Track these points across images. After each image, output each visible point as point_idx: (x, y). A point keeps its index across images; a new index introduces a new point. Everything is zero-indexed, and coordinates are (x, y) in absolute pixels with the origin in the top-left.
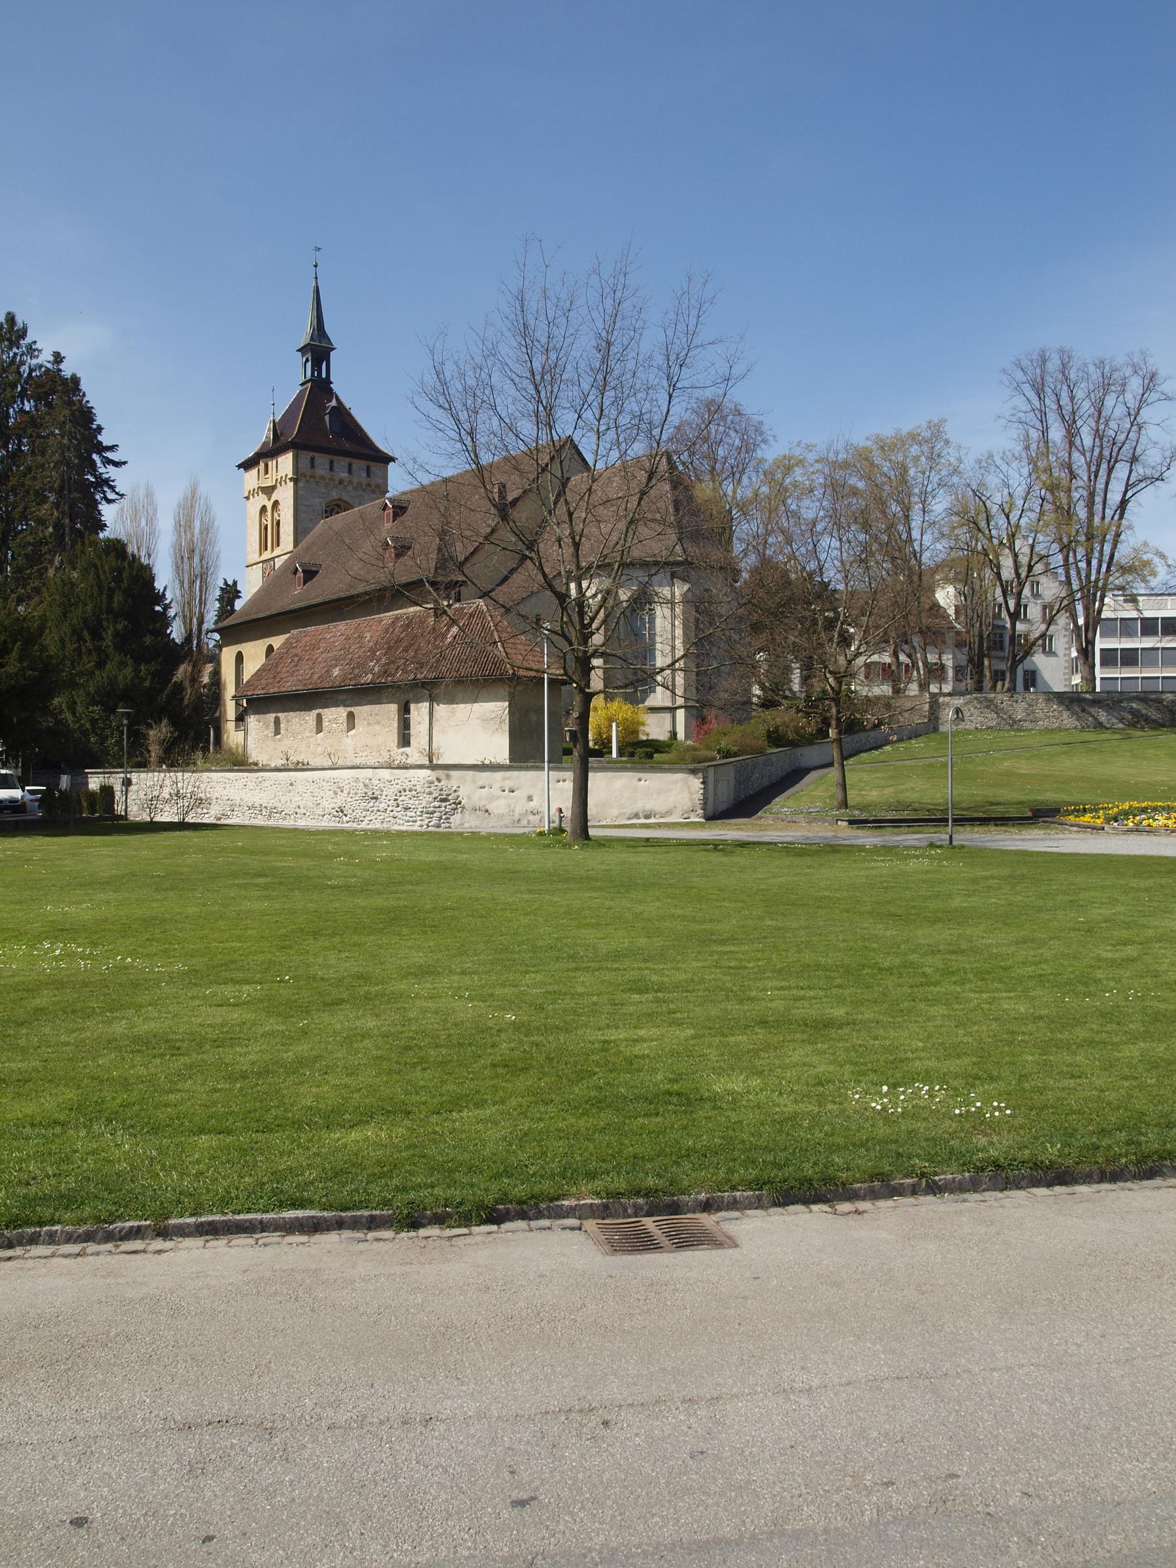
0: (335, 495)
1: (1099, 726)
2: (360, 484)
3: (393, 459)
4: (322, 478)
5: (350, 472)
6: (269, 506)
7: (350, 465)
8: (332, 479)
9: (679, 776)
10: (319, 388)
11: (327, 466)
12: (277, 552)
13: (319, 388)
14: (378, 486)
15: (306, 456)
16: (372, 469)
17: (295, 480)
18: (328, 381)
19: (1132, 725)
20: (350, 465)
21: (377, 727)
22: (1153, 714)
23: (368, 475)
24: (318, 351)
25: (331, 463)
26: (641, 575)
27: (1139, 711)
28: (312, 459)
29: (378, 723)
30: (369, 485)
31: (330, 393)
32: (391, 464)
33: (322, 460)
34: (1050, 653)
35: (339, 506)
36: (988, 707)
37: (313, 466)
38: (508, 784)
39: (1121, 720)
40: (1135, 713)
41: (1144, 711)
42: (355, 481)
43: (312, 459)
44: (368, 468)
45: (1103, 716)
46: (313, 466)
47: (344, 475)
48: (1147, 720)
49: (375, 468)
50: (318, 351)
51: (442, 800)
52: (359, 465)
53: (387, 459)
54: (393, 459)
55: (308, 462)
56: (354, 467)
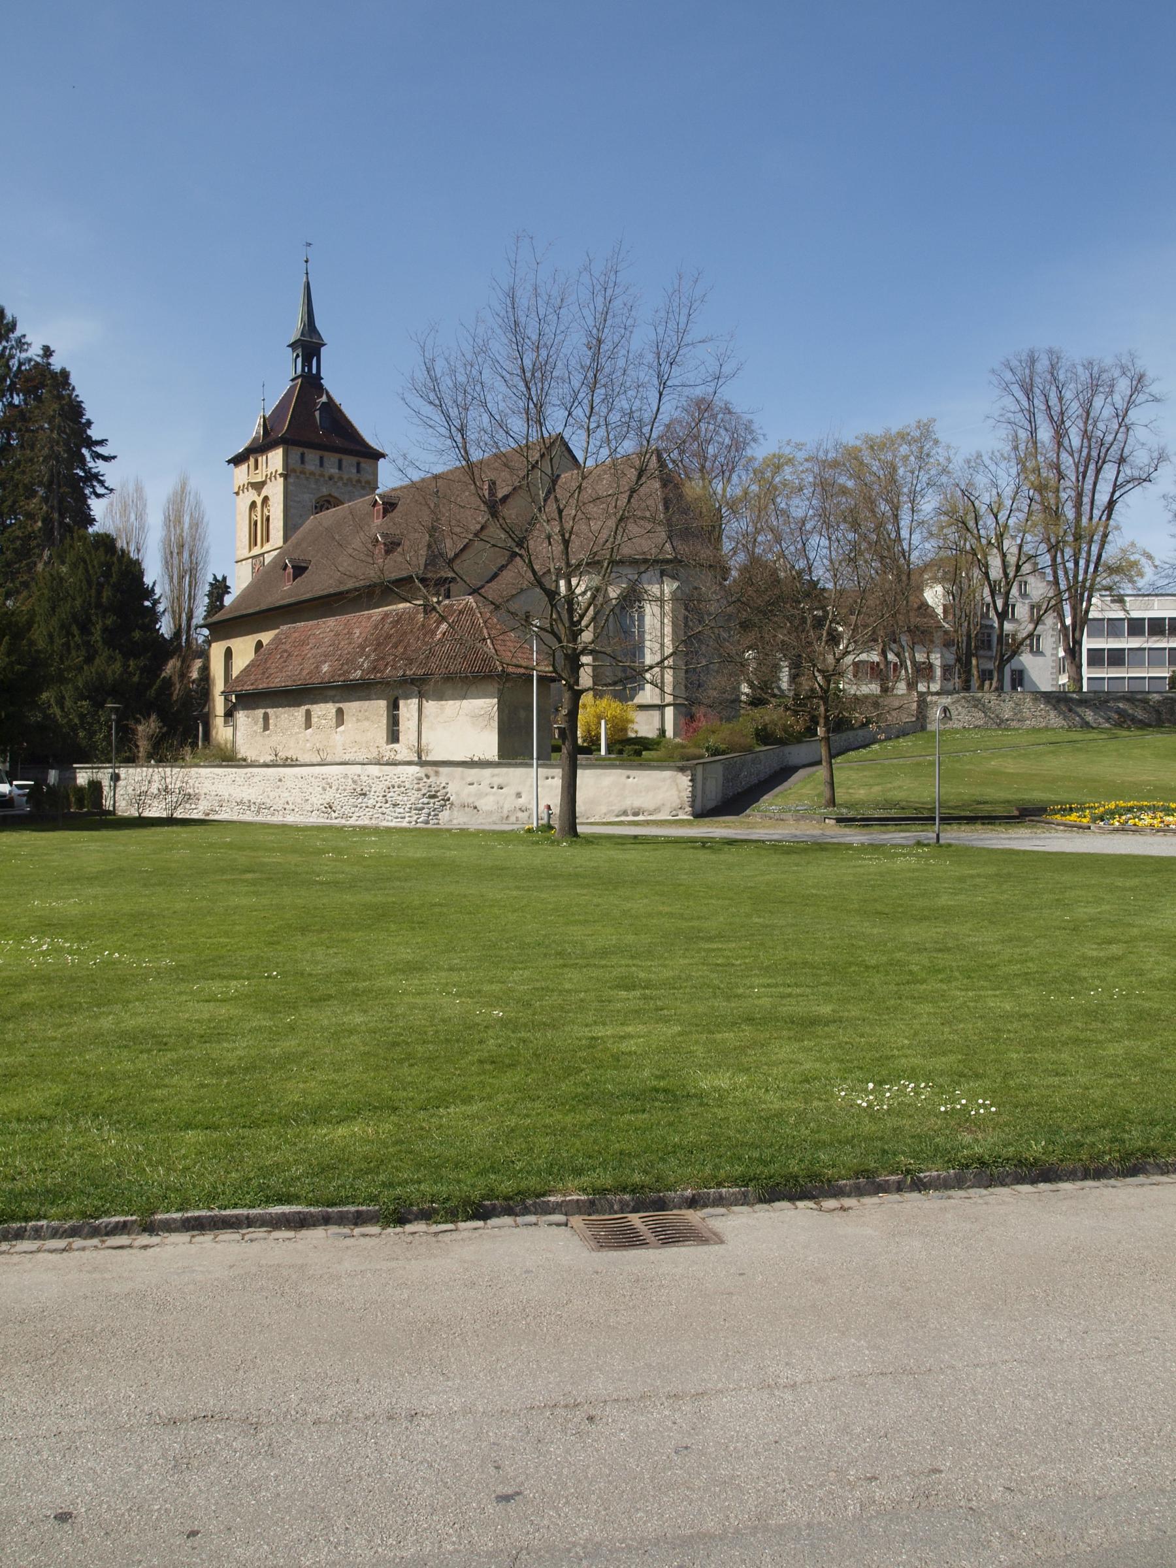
0: (325, 491)
1: (1086, 725)
2: (350, 480)
3: (383, 456)
5: (340, 468)
6: (259, 501)
7: (340, 461)
8: (322, 475)
9: (667, 774)
10: (310, 383)
11: (318, 462)
13: (310, 383)
14: (368, 482)
16: (363, 465)
18: (318, 377)
19: (1119, 725)
21: (366, 724)
22: (1140, 714)
23: (358, 471)
24: (309, 347)
25: (321, 458)
26: (630, 573)
27: (1125, 711)
28: (303, 455)
29: (367, 719)
32: (382, 460)
35: (329, 502)
36: (975, 706)
37: (303, 462)
38: (497, 781)
39: (1108, 720)
40: (1121, 713)
41: (1130, 711)
42: (345, 477)
43: (303, 455)
44: (358, 464)
45: (1090, 716)
46: (303, 462)
47: (334, 471)
48: (1134, 719)
50: (309, 347)
51: (431, 797)
54: (383, 456)
55: (298, 458)
56: (344, 463)
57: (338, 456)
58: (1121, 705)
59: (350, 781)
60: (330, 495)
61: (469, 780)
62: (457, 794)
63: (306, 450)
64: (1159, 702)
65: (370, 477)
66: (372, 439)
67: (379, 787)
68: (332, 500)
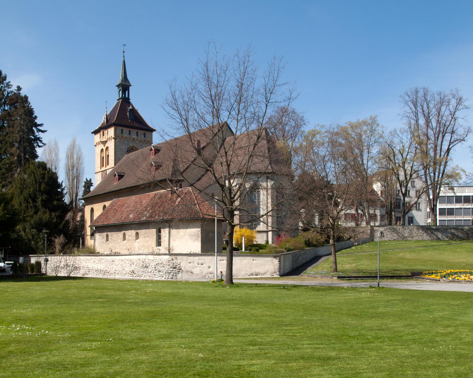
0: (131, 145)
1: (438, 239)
2: (141, 140)
3: (154, 130)
4: (126, 138)
5: (137, 135)
6: (104, 149)
7: (137, 133)
8: (130, 138)
10: (125, 101)
11: (136, 134)
12: (108, 167)
13: (125, 101)
14: (148, 141)
15: (120, 129)
16: (146, 134)
17: (115, 139)
18: (128, 99)
19: (452, 239)
20: (137, 133)
21: (148, 238)
22: (460, 235)
23: (145, 137)
24: (125, 87)
25: (130, 131)
27: (454, 233)
28: (122, 130)
29: (148, 236)
30: (145, 141)
31: (129, 103)
32: (154, 132)
33: (126, 130)
34: (419, 210)
35: (133, 149)
36: (394, 231)
37: (122, 133)
38: (200, 262)
39: (447, 237)
40: (453, 234)
41: (456, 234)
42: (139, 139)
44: (145, 134)
45: (440, 235)
46: (122, 133)
47: (135, 136)
48: (457, 237)
49: (147, 133)
50: (125, 87)
51: (174, 268)
52: (141, 132)
53: (152, 130)
54: (154, 130)
56: (139, 134)
57: (136, 130)
58: (452, 231)
59: (141, 262)
60: (133, 146)
61: (189, 261)
62: (185, 267)
63: (123, 128)
64: (468, 230)
65: (149, 139)
66: (150, 124)
67: (153, 264)
68: (134, 148)
